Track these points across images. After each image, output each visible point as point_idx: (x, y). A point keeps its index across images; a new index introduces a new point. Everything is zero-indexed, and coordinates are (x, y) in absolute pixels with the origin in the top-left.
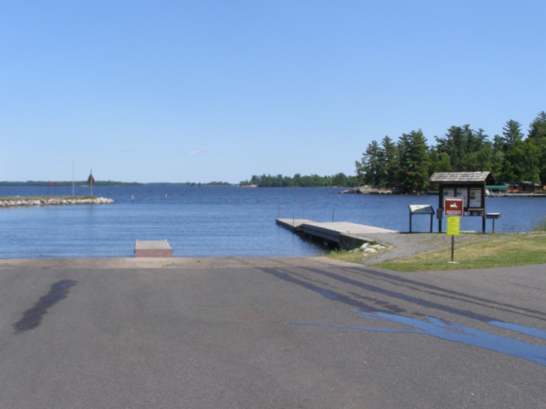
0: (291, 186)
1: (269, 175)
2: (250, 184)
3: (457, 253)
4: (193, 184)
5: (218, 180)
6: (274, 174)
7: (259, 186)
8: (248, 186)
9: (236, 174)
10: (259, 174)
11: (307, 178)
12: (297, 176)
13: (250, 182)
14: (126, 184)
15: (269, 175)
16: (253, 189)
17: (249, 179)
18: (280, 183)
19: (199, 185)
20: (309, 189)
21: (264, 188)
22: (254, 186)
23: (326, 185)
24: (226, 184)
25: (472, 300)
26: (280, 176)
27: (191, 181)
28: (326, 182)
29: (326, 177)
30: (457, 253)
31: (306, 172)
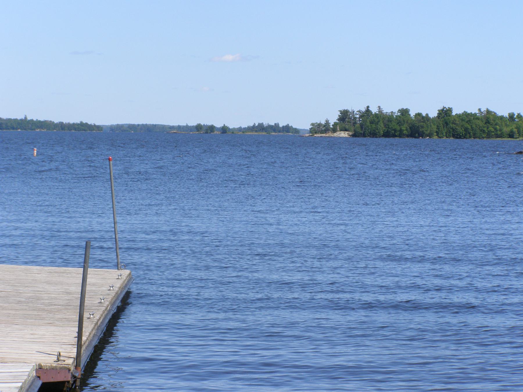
0: (430, 135)
1: (427, 115)
2: (334, 130)
3: (108, 205)
4: (212, 128)
5: (269, 121)
6: (391, 107)
7: (354, 136)
8: (330, 134)
9: (307, 109)
10: (356, 107)
11: (466, 117)
12: (445, 113)
13: (335, 124)
14: (62, 126)
15: (427, 115)
16: (333, 144)
17: (333, 119)
18: (404, 127)
19: (224, 130)
20: (467, 143)
21: (368, 140)
22: (344, 134)
23: (511, 135)
24: (287, 129)
25: (470, 357)
26: (404, 112)
27: (206, 122)
28: (513, 127)
29: (511, 117)
30: (108, 205)
31: (465, 103)
